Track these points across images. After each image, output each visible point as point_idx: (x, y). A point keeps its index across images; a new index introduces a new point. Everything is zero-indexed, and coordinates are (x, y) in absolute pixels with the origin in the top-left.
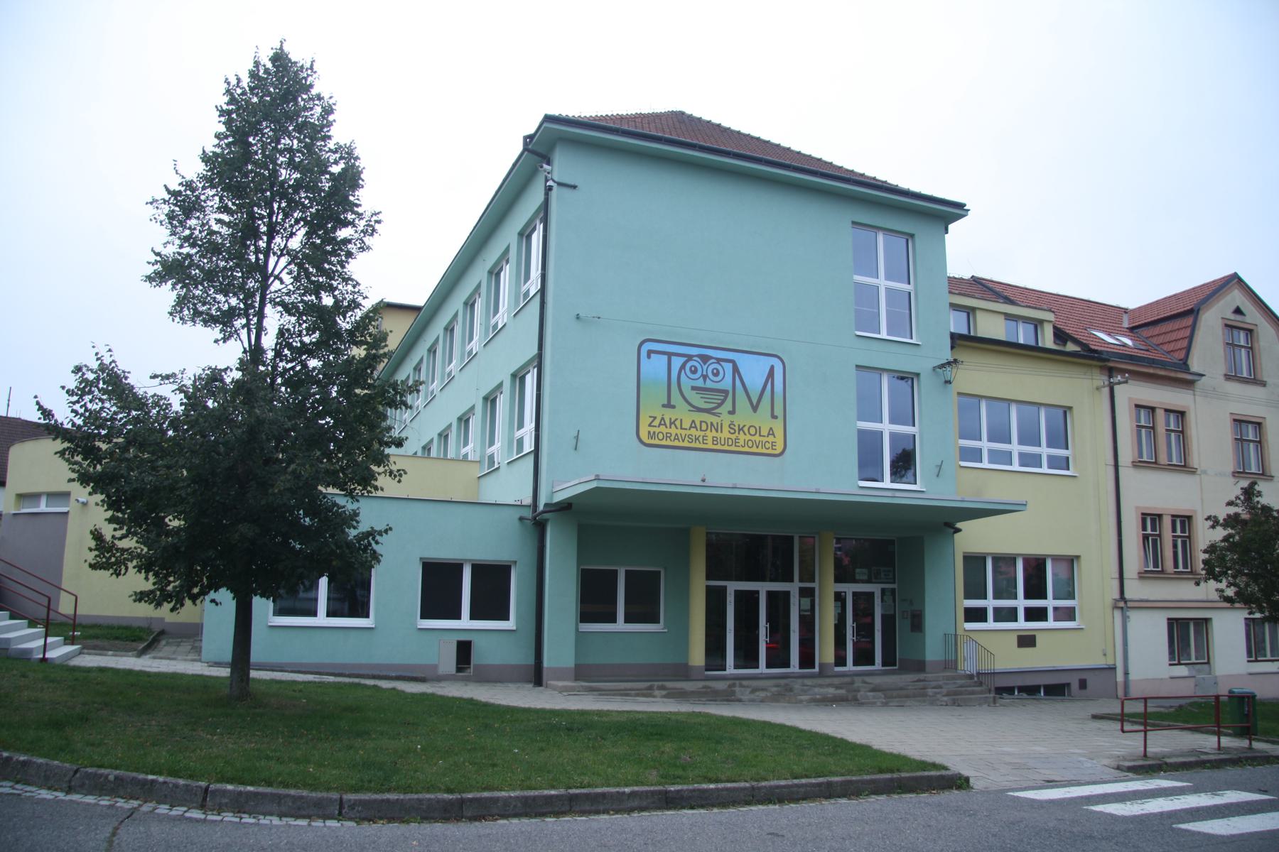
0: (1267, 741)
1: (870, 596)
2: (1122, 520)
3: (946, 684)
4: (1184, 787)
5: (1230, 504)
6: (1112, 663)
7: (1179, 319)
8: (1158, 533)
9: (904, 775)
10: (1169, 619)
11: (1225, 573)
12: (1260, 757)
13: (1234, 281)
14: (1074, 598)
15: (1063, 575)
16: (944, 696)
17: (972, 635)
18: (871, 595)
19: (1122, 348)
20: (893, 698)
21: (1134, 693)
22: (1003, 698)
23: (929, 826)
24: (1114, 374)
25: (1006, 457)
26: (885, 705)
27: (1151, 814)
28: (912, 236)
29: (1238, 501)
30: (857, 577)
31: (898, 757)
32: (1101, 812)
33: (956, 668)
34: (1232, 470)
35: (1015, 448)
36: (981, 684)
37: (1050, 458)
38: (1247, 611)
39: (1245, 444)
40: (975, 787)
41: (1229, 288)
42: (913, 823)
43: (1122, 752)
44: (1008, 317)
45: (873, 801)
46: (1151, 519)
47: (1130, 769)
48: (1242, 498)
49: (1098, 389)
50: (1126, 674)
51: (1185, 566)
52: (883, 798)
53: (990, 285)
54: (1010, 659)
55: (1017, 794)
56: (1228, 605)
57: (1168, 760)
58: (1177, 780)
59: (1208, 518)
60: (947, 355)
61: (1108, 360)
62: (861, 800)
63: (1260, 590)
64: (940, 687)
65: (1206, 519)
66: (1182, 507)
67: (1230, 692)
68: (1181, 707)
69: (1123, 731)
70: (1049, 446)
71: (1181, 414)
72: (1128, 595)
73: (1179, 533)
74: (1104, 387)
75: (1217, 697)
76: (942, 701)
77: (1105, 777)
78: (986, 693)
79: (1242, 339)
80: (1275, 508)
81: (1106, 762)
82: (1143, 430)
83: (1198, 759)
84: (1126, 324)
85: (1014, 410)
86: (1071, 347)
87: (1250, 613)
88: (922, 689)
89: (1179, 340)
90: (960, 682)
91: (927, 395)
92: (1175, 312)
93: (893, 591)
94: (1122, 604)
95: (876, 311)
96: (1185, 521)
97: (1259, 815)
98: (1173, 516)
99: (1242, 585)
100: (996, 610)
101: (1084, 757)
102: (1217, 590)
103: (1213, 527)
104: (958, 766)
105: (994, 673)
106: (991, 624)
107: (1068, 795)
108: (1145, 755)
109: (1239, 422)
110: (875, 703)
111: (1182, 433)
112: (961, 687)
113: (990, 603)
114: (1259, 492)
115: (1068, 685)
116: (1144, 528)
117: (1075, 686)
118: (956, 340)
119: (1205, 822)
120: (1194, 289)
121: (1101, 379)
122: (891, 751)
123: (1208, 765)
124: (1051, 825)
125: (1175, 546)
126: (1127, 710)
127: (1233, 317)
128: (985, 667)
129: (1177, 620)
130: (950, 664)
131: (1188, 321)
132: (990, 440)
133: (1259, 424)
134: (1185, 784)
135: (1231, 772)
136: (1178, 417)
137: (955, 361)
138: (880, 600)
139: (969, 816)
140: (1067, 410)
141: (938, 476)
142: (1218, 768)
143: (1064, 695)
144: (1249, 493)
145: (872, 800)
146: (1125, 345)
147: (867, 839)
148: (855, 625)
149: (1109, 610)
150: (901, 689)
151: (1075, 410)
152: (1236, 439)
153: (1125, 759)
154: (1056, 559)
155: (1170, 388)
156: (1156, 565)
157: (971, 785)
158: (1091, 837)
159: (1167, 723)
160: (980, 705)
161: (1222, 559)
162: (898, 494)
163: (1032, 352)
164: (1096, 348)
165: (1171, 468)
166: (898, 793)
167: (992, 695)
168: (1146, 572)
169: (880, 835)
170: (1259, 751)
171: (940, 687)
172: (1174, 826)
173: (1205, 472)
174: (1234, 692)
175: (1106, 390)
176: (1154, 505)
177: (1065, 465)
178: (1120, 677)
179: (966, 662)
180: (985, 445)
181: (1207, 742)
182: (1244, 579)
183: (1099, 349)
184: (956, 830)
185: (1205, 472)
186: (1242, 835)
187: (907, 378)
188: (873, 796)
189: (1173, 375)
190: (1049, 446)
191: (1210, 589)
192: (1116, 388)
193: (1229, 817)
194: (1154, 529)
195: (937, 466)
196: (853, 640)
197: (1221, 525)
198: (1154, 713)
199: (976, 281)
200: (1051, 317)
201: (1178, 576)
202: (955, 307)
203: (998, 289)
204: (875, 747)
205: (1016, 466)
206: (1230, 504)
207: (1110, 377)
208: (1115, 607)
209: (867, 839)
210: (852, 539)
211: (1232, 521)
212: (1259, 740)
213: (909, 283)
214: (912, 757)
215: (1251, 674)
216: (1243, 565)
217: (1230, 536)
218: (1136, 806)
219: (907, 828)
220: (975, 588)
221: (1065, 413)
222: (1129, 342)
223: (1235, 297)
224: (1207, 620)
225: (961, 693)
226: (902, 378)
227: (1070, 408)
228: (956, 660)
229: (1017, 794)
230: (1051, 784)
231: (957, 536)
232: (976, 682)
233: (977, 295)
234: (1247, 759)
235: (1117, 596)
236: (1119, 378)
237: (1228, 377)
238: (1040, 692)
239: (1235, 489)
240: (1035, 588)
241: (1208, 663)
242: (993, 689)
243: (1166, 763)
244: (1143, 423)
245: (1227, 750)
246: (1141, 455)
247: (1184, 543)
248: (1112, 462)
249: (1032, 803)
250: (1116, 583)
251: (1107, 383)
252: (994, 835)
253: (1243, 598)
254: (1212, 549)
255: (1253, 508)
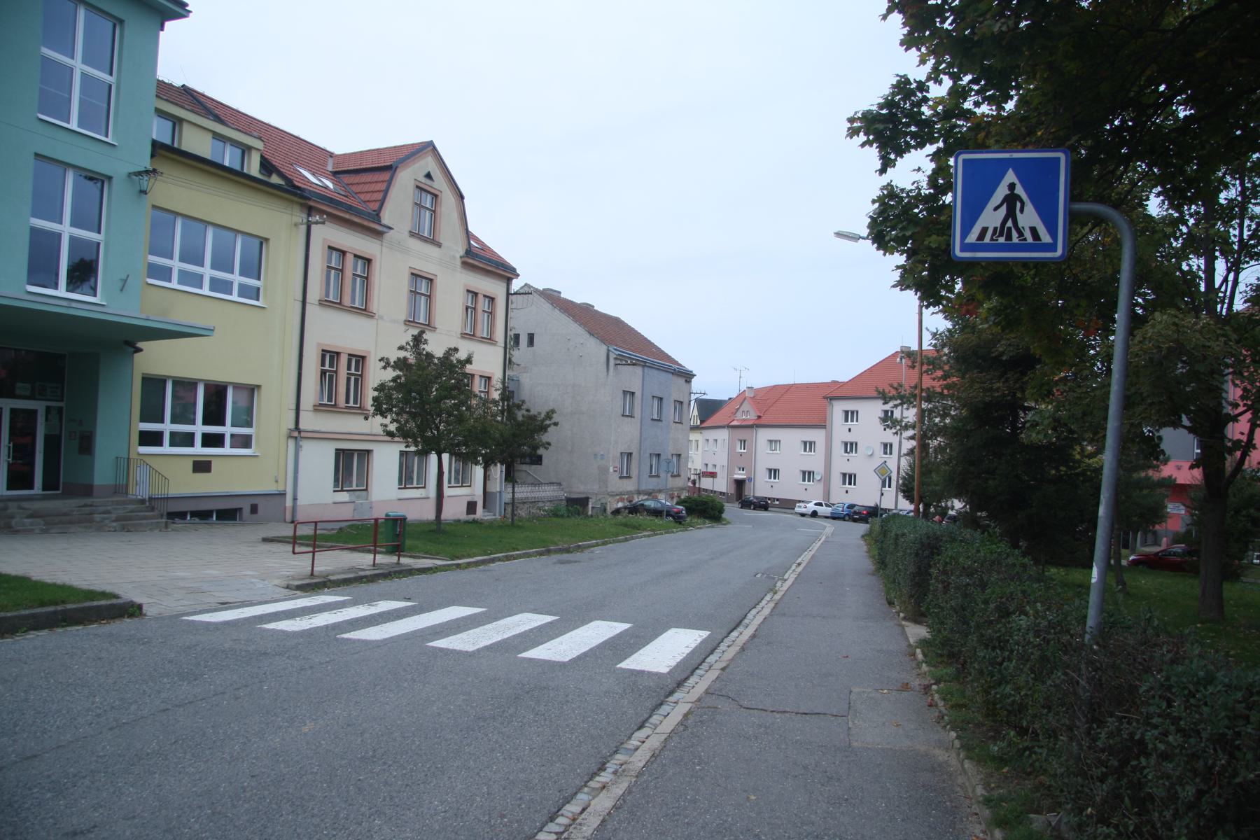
0: (410, 557)
1: (32, 414)
2: (304, 354)
3: (115, 509)
4: (344, 601)
5: (401, 348)
6: (283, 489)
7: (378, 173)
8: (335, 369)
9: (69, 606)
10: (337, 450)
11: (390, 410)
12: (406, 570)
13: (429, 148)
14: (252, 427)
15: (243, 403)
16: (114, 521)
17: (147, 460)
18: (34, 412)
19: (323, 189)
20: (54, 525)
21: (300, 517)
22: (174, 523)
23: (100, 659)
24: (313, 214)
25: (197, 280)
26: (45, 532)
27: (318, 627)
28: (121, 22)
29: (408, 347)
30: (18, 392)
31: (63, 587)
32: (273, 629)
33: (127, 493)
34: (404, 318)
35: (207, 272)
36: (153, 509)
37: (242, 286)
38: (405, 445)
39: (418, 296)
40: (148, 614)
41: (425, 153)
42: (81, 657)
43: (291, 572)
44: (217, 136)
45: (33, 638)
46: (328, 356)
47: (299, 588)
48: (412, 344)
49: (296, 225)
50: (295, 499)
51: (355, 402)
52: (44, 633)
53: (202, 99)
54: (185, 484)
55: (191, 618)
56: (389, 438)
57: (332, 578)
58: (338, 595)
59: (382, 360)
60: (145, 162)
61: (309, 199)
62: (17, 638)
63: (417, 426)
64: (108, 512)
65: (380, 360)
66: (358, 347)
67: (387, 515)
68: (341, 529)
69: (294, 553)
70: (242, 274)
71: (368, 261)
72: (302, 426)
73: (353, 371)
74: (302, 224)
75: (376, 520)
76: (110, 527)
77: (276, 596)
78: (157, 518)
79: (427, 200)
80: (437, 356)
81: (277, 582)
82: (333, 272)
83: (357, 575)
84: (330, 168)
85: (210, 233)
86: (275, 179)
87: (407, 447)
88: (87, 514)
89: (376, 192)
90: (131, 507)
91: (117, 201)
92: (376, 165)
93: (60, 410)
94: (296, 434)
95: (68, 96)
96: (359, 360)
97: (405, 620)
98: (349, 355)
99: (403, 423)
100: (173, 434)
101: (257, 578)
102: (381, 425)
103: (385, 368)
104: (130, 594)
105: (168, 498)
106: (166, 449)
107: (242, 616)
108: (312, 574)
109: (416, 276)
110: (33, 530)
111: (366, 279)
112: (132, 512)
113: (167, 427)
114: (426, 340)
115: (240, 509)
116: (323, 364)
117: (246, 511)
118: (158, 149)
119: (363, 630)
120: (395, 147)
121: (299, 216)
122: (54, 581)
123: (364, 580)
124: (227, 646)
125: (348, 380)
126: (299, 533)
127: (424, 180)
128: (158, 492)
129: (343, 450)
130: (120, 489)
131: (386, 176)
132: (182, 260)
133: (431, 280)
134: (346, 598)
135: (383, 585)
136: (365, 263)
137: (154, 171)
138: (44, 418)
139: (143, 644)
140: (263, 241)
141: (122, 290)
142: (372, 582)
143: (236, 520)
144: (418, 340)
145: (32, 636)
146: (326, 187)
147: (26, 680)
148: (11, 445)
149: (283, 439)
150: (65, 514)
151: (271, 243)
152: (411, 291)
153: (294, 579)
154: (238, 387)
155: (361, 236)
156: (330, 399)
157: (144, 612)
158: (265, 654)
159: (330, 544)
160: (151, 530)
161: (389, 397)
162: (74, 305)
163: (236, 177)
164: (300, 185)
165: (353, 310)
166: (63, 627)
167: (164, 520)
168: (321, 405)
169: (42, 674)
170: (407, 565)
171: (108, 512)
172: (338, 636)
173: (382, 318)
174: (389, 516)
175: (303, 228)
176: (334, 343)
177: (255, 296)
178: (289, 503)
179: (138, 487)
180: (176, 264)
181: (364, 560)
182: (405, 416)
183: (303, 186)
184: (130, 659)
185: (382, 318)
186: (392, 638)
187: (97, 179)
188: (32, 632)
189: (366, 223)
190: (242, 274)
191: (376, 424)
192: (314, 227)
193: (671, 670)
194: (331, 365)
195: (121, 280)
196: (8, 462)
197: (392, 367)
198: (322, 535)
199: (186, 90)
200: (259, 144)
201: (349, 411)
202: (161, 113)
203: (209, 105)
204: (34, 579)
205: (206, 291)
206: (401, 348)
207: (309, 215)
208: (290, 437)
209: (26, 680)
210: (10, 349)
211: (401, 364)
212: (405, 556)
213: (111, 74)
214: (79, 587)
215: (400, 500)
216: (406, 404)
217: (398, 377)
218: (304, 621)
219: (74, 662)
220: (152, 411)
221: (261, 244)
222: (330, 185)
223: (428, 163)
224: (369, 452)
225: (130, 519)
226: (91, 179)
227: (267, 240)
228: (127, 486)
229: (191, 618)
230: (225, 605)
231: (136, 355)
232: (147, 507)
233: (186, 106)
234: (395, 572)
235: (292, 426)
236: (318, 218)
237: (412, 234)
238: (212, 517)
239: (407, 336)
240: (215, 414)
241: (366, 490)
242: (165, 513)
243: (330, 581)
244: (333, 265)
245: (381, 566)
246: (327, 294)
247: (356, 381)
248: (300, 298)
249: (207, 625)
250: (292, 414)
251: (305, 221)
252: (170, 662)
253: (403, 433)
254: (381, 388)
255: (419, 354)
